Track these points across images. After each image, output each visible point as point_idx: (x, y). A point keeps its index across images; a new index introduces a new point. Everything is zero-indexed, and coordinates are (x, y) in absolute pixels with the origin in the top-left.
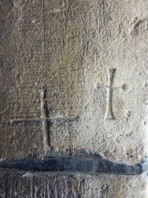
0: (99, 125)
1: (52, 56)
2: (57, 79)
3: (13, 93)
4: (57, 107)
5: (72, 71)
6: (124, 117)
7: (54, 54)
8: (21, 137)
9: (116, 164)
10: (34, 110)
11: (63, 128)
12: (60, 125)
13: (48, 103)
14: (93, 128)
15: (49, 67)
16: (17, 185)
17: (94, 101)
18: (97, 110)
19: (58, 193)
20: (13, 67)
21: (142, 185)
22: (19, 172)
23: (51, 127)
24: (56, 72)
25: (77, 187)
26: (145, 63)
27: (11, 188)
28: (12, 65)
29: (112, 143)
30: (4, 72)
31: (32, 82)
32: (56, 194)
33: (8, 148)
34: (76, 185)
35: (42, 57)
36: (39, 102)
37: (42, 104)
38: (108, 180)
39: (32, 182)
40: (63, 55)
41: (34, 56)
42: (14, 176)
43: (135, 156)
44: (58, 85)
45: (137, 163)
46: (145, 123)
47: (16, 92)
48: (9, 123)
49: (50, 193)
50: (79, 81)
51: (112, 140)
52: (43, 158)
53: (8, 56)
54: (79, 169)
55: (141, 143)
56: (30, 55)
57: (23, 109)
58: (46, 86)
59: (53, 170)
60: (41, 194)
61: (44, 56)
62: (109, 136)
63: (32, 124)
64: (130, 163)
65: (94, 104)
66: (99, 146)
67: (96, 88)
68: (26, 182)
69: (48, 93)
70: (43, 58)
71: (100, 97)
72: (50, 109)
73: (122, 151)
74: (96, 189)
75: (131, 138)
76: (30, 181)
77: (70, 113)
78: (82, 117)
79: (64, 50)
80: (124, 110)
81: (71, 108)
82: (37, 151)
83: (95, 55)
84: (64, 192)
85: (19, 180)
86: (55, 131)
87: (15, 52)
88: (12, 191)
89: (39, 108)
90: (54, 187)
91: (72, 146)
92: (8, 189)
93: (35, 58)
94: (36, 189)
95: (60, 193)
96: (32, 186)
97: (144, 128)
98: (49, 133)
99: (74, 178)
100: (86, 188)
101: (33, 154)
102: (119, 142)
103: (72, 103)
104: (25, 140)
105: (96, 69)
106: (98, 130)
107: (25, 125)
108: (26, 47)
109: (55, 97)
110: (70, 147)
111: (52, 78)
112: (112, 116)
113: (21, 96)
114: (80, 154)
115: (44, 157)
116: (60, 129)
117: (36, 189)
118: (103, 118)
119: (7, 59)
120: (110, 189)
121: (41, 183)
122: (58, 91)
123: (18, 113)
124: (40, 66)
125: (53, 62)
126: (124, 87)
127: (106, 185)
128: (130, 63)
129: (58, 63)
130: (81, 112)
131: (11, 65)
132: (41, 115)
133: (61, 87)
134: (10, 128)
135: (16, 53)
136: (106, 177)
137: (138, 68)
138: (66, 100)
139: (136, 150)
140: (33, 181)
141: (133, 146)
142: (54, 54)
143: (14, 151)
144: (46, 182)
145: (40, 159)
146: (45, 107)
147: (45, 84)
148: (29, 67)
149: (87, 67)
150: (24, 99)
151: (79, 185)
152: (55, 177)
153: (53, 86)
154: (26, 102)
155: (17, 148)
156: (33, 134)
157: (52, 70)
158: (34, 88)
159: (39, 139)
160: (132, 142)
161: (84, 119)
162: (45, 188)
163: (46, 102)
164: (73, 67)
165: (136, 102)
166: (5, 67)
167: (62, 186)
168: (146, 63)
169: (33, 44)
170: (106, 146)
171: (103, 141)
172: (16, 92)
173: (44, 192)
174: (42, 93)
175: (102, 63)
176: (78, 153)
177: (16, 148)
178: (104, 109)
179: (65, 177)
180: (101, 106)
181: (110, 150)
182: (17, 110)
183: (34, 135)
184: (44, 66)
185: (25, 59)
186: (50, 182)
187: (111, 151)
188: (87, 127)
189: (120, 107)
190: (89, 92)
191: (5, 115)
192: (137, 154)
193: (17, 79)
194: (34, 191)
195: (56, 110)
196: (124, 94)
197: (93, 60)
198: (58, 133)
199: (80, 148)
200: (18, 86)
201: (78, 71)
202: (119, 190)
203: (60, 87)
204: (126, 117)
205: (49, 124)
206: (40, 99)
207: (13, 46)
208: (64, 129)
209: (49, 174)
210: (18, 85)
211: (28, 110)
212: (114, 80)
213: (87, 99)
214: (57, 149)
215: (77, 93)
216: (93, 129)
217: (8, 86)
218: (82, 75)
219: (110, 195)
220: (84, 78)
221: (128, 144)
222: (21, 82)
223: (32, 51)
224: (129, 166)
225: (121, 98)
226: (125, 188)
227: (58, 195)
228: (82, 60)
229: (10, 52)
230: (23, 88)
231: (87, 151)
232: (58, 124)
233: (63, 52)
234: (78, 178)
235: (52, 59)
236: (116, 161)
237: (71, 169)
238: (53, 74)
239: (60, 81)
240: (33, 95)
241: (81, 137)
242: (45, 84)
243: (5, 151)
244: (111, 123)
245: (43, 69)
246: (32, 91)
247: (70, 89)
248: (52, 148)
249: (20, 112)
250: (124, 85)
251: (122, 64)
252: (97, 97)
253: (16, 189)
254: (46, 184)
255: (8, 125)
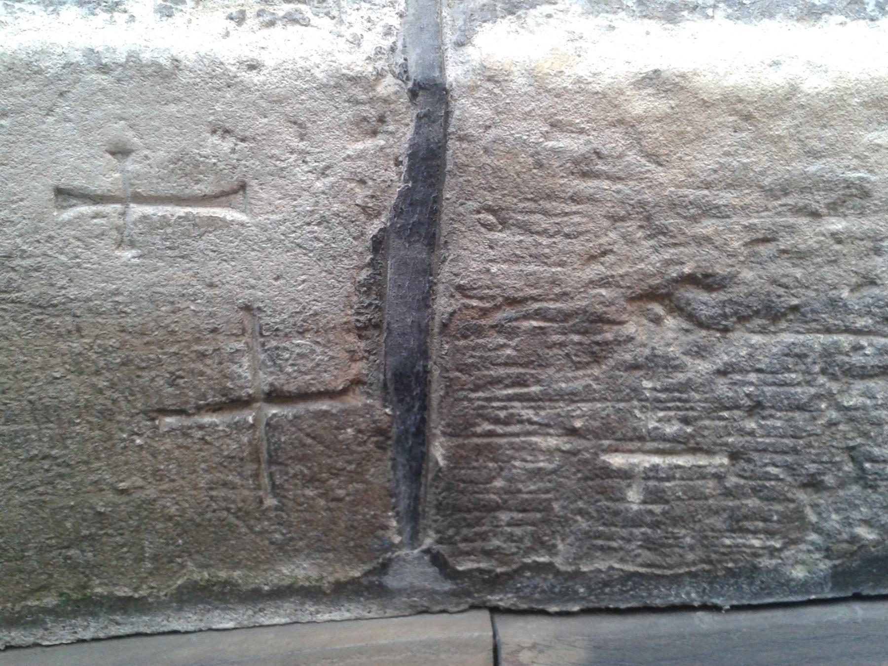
0: (269, 240)
1: (40, 399)
2: (116, 379)
3: (177, 503)
4: (215, 374)
5: (83, 337)
6: (233, 151)
7: (32, 394)
8: (321, 473)
9: (406, 181)
10: (229, 442)
11: (286, 355)
12: (275, 363)
13: (202, 402)
14: (280, 259)
15: (78, 407)
16: (471, 482)
17: (183, 257)
18: (215, 249)
19: (499, 365)
20: (92, 507)
21: (489, 80)
22: (430, 476)
23: (285, 388)
24: (94, 386)
25: (481, 309)
26: (17, 79)
27: (481, 496)
28: (86, 510)
29: (333, 192)
30: (110, 531)
31: (134, 452)
32: (502, 371)
33: (355, 509)
34: (474, 313)
35: (47, 428)
36: (201, 427)
37: (207, 419)
38: (461, 209)
39: (460, 441)
40: (29, 367)
41: (46, 450)
42: (444, 490)
43: (380, 107)
44: (139, 376)
45: (405, 99)
46: (252, 67)
47: (174, 495)
48: (277, 508)
49: (500, 389)
50: (114, 312)
51: (323, 193)
52: (387, 410)
53: (59, 523)
54: (426, 300)
55: (332, 83)
56: (46, 464)
57: (226, 471)
58: (145, 412)
59: (424, 379)
60: (502, 414)
61: (43, 423)
62: (305, 203)
63: (275, 443)
64: (407, 125)
65: (194, 258)
66: (344, 239)
67: (134, 252)
68: (462, 456)
69: (169, 403)
70: (51, 425)
71: (166, 240)
72: (223, 396)
73: (360, 156)
74: (491, 247)
75: (315, 122)
76: (458, 446)
77: (233, 335)
78: (245, 296)
79: (12, 366)
80: (207, 151)
81: (214, 331)
82: (363, 426)
83: (15, 263)
84: (495, 349)
85: (454, 476)
86: (295, 378)
87: (42, 504)
88: (488, 493)
89: (220, 428)
90: (479, 379)
91: (345, 323)
92: (484, 506)
93: (52, 448)
94: (487, 427)
95: (499, 361)
96: (476, 440)
97: (274, 73)
98: (304, 396)
99: (450, 320)
100: (486, 280)
101: (374, 436)
102: (328, 167)
103: (196, 328)
104: (329, 461)
105: (63, 258)
106: (286, 242)
107: (280, 464)
108: (21, 476)
109: (181, 381)
110: (349, 331)
111: (116, 395)
112: (235, 192)
113: (187, 480)
114: (374, 297)
115: (386, 407)
116: (290, 362)
117: (487, 427)
118: (242, 225)
119: (68, 525)
120: (495, 200)
121: (464, 415)
122: (158, 376)
123: (242, 486)
124: (78, 434)
125: (58, 395)
126: (121, 151)
127: (479, 212)
128: (28, 136)
129: (59, 381)
130: (229, 301)
131: (84, 513)
132: (246, 422)
133: (144, 365)
134: (291, 504)
135: (45, 502)
136: (453, 216)
137: (42, 104)
138: (188, 347)
139: (358, 102)
140: (458, 436)
141: (344, 116)
142: (32, 394)
143: (366, 491)
144: (462, 400)
145: (387, 419)
146: (216, 408)
147: (137, 414)
148: (86, 463)
149: (62, 288)
150: (195, 471)
151: (475, 303)
152: (446, 375)
153: (143, 391)
154: (203, 466)
155: (357, 483)
156: (309, 441)
157: (86, 397)
158: (156, 445)
159: (325, 423)
160: (327, 119)
161: (253, 287)
162: (480, 403)
163: (199, 409)
164: (69, 332)
165: (172, 108)
166: (93, 530)
167: (474, 354)
168: (17, 74)
169: (7, 455)
170: (345, 214)
171: (325, 224)
172: (174, 495)
173: (495, 404)
174: (171, 420)
175: (38, 237)
176: (370, 304)
177: (355, 485)
178: (209, 225)
179: (446, 346)
180: (201, 236)
181: (359, 202)
182: (233, 488)
183: (314, 438)
184: (78, 421)
185: (61, 476)
186: (462, 389)
187: (361, 194)
188: (277, 279)
189: (196, 166)
190: (152, 277)
191: (252, 522)
192: (371, 101)
193: (130, 494)
194: (491, 434)
195: (225, 377)
196: (147, 152)
197: (36, 270)
198: (303, 369)
199: (355, 299)
200: (151, 492)
201: (78, 317)
202: (500, 170)
203: (143, 369)
204: (232, 145)
205: (275, 396)
206: (190, 428)
207: (24, 512)
208: (288, 350)
209: (436, 393)
210: (148, 492)
211: (233, 457)
212: (99, 192)
213: (179, 283)
214: (358, 368)
215: (159, 316)
216: (287, 257)
217: (156, 519)
218: (91, 304)
219: (515, 200)
220: (103, 295)
221: (337, 133)
222: (140, 483)
223: (31, 459)
224: (417, 133)
225: (160, 165)
226: (496, 146)
227: (506, 364)
228: (40, 306)
229: (43, 518)
230: (158, 476)
231: (364, 274)
232: (272, 369)
233: (20, 366)
234: (451, 305)
235: (48, 399)
236: (395, 178)
237: (424, 331)
238: (100, 391)
239: (122, 372)
240: (179, 447)
241: (312, 297)
242: (137, 414)
243: (364, 515)
244: (261, 199)
245: (89, 422)
246: (166, 449)
247: (147, 339)
248: (357, 382)
249: (238, 480)
250: (113, 153)
251: (33, 166)
252: (170, 248)
253: (482, 483)
254: (470, 400)
255: (283, 511)
